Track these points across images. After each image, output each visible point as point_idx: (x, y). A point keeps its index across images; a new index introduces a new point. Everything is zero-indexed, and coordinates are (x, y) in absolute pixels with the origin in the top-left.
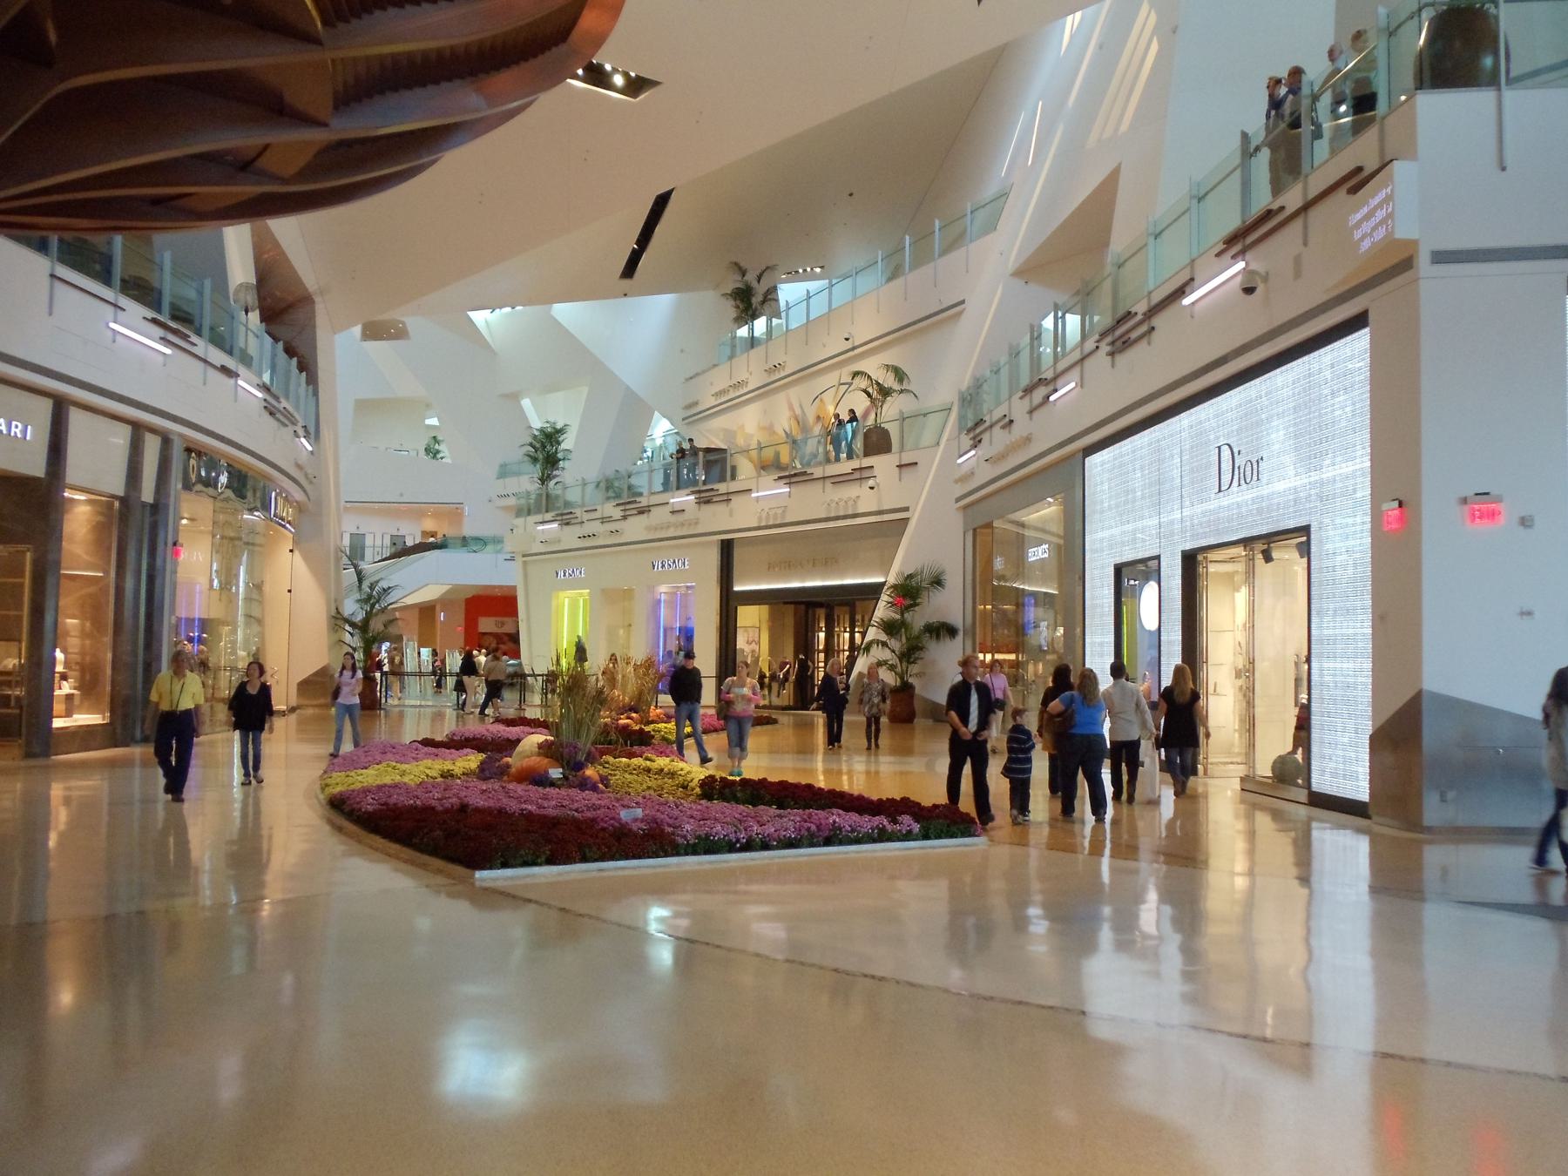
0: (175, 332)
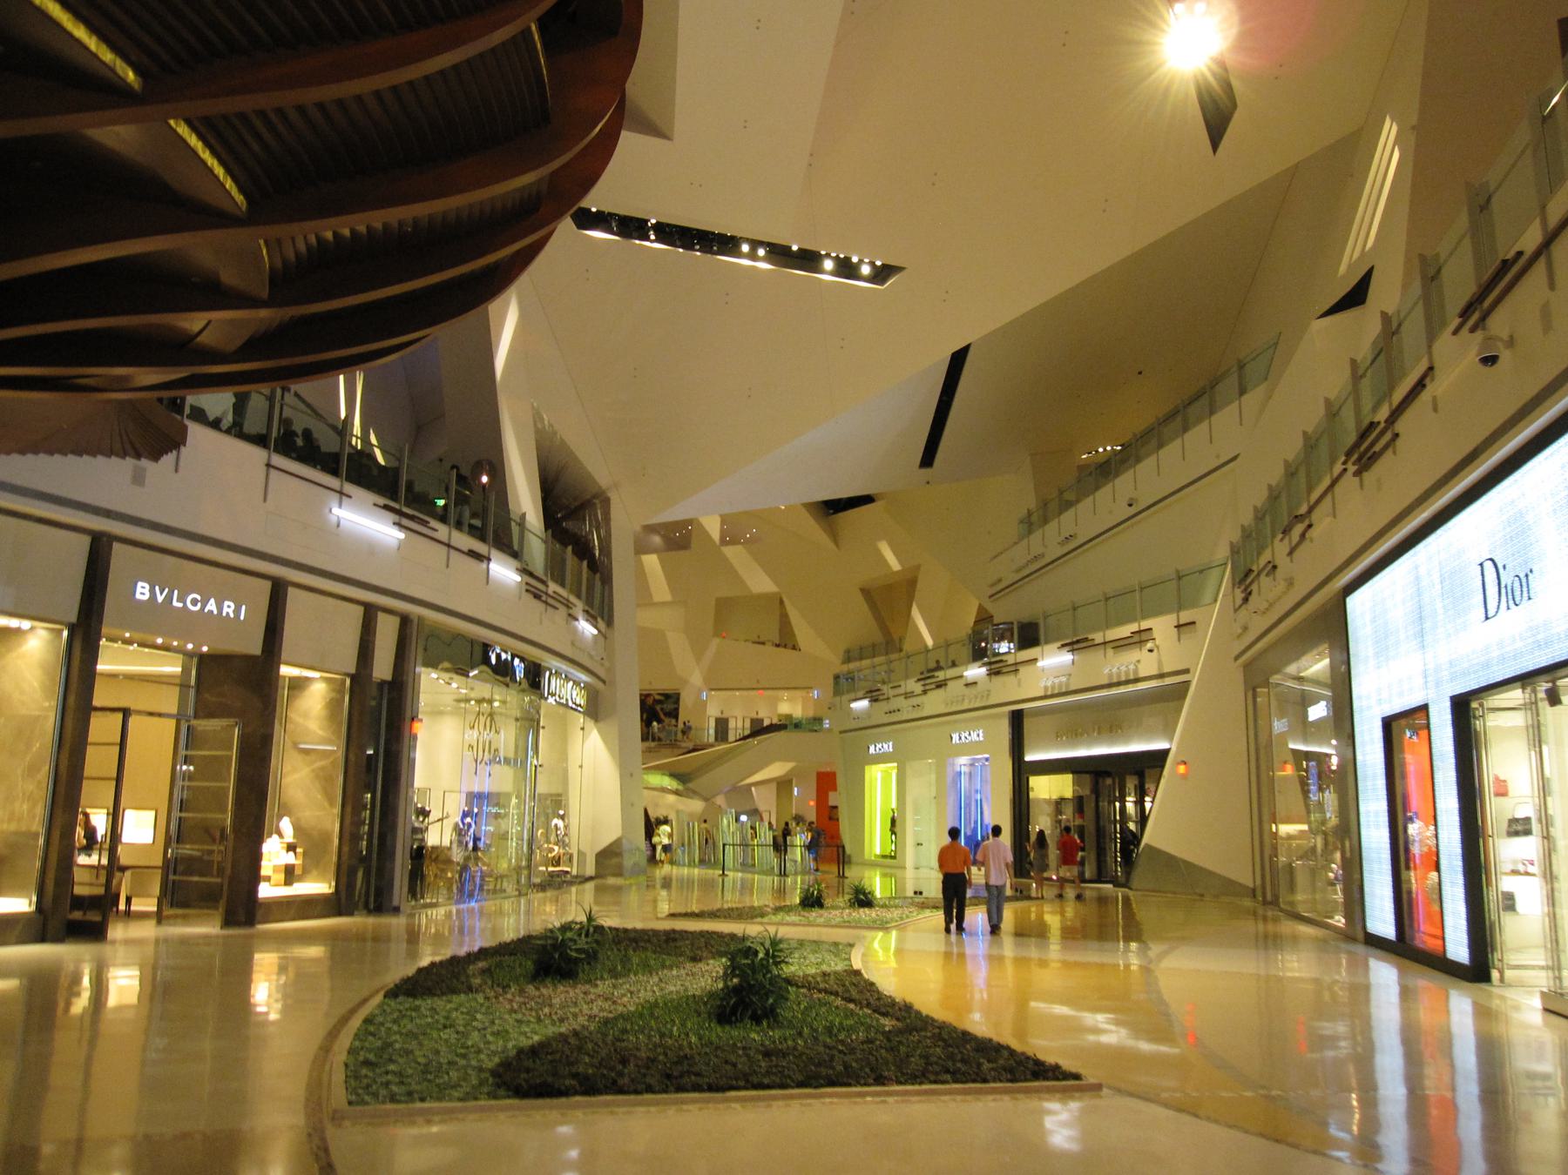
0: (412, 518)
